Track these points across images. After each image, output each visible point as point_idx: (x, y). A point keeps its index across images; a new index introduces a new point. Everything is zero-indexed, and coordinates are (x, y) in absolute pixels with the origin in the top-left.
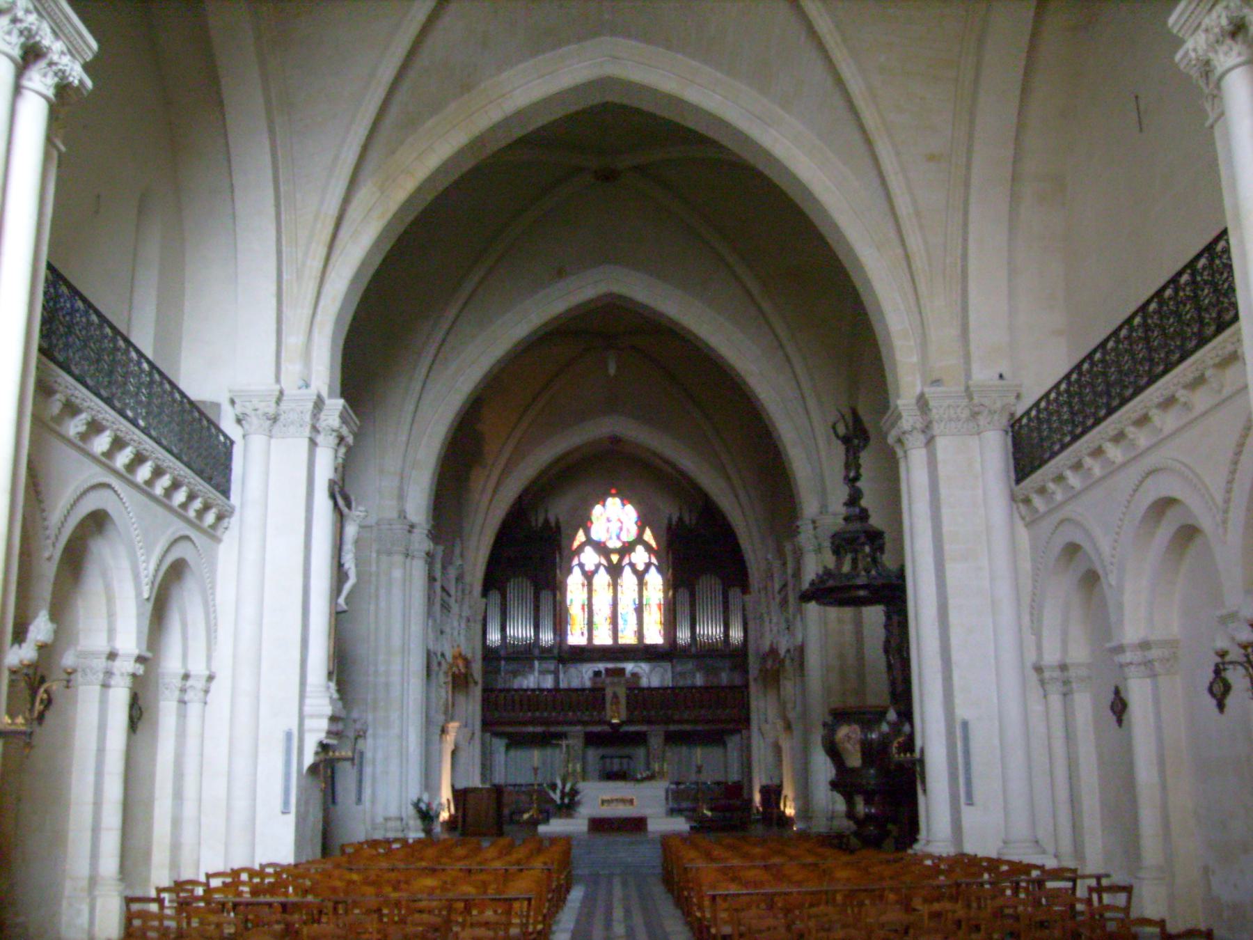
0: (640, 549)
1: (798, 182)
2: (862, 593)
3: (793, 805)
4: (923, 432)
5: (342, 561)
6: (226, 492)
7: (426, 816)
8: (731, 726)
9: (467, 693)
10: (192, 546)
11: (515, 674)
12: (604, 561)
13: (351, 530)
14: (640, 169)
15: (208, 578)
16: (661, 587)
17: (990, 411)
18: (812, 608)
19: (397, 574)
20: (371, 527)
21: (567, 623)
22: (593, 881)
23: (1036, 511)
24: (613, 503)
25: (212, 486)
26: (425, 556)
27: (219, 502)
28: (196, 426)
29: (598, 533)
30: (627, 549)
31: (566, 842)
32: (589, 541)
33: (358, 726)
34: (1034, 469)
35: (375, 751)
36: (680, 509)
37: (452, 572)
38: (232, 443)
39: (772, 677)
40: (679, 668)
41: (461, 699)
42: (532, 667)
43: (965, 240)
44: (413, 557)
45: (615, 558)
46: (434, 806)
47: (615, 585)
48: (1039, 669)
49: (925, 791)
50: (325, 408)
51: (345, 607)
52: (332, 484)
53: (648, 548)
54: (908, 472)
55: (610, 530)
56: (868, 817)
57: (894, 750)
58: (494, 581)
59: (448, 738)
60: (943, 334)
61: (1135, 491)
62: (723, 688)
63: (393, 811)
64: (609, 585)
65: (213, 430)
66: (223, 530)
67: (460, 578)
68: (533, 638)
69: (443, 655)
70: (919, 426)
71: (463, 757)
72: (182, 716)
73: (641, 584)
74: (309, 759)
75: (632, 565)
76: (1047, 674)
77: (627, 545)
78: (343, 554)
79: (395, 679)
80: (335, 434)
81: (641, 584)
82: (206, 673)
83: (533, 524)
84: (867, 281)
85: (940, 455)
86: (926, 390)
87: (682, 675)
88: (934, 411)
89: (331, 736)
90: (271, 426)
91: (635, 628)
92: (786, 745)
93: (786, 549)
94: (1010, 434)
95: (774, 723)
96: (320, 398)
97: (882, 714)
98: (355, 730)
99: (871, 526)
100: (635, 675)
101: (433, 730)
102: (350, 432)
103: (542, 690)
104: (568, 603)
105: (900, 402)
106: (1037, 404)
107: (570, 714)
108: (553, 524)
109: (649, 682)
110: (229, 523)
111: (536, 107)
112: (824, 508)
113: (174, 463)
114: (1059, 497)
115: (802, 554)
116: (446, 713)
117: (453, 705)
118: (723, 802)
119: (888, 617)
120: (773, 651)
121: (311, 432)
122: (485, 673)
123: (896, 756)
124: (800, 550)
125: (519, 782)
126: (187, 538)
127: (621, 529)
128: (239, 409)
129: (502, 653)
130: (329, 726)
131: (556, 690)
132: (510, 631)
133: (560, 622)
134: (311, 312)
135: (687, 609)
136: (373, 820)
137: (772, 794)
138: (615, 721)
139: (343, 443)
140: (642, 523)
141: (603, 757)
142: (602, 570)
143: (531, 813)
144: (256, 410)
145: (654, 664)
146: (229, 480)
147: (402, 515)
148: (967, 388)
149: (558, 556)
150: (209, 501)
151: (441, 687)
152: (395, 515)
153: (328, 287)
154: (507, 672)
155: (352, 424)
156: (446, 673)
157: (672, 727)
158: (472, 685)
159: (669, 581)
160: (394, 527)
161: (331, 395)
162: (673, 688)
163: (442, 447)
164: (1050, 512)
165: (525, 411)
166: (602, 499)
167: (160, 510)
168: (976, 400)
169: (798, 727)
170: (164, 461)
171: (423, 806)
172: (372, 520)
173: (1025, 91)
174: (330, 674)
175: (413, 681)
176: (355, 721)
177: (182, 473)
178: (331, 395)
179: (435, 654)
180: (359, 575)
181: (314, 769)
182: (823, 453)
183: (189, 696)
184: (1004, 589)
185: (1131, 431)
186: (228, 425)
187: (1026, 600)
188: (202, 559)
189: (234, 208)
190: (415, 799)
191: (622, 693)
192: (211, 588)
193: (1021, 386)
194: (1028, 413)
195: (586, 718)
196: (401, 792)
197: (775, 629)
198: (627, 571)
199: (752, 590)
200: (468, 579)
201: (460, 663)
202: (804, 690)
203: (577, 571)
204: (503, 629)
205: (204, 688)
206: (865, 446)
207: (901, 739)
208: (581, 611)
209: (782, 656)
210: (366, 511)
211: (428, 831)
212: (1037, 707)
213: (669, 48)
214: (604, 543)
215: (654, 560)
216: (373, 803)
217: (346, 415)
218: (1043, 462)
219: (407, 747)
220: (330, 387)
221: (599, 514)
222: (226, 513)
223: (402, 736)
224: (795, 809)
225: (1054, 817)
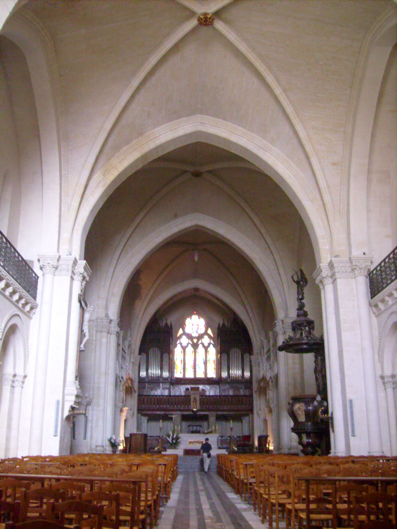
0: (206, 337)
2: (305, 346)
3: (272, 445)
4: (331, 277)
5: (83, 329)
6: (35, 298)
7: (114, 445)
8: (245, 412)
9: (131, 396)
11: (152, 389)
13: (87, 316)
15: (26, 333)
16: (215, 353)
17: (360, 268)
18: (282, 354)
19: (104, 340)
21: (174, 368)
22: (187, 473)
23: (380, 309)
24: (195, 317)
25: (29, 294)
26: (116, 333)
27: (32, 301)
28: (24, 268)
29: (188, 329)
30: (200, 337)
31: (176, 457)
32: (184, 333)
33: (88, 399)
34: (379, 292)
35: (92, 416)
36: (223, 320)
37: (127, 343)
38: (38, 277)
39: (263, 391)
40: (222, 388)
41: (129, 399)
42: (159, 386)
44: (111, 334)
45: (195, 341)
46: (118, 441)
47: (195, 352)
48: (382, 377)
49: (333, 431)
50: (78, 264)
51: (84, 349)
52: (80, 296)
54: (325, 294)
55: (193, 329)
56: (308, 444)
57: (320, 413)
58: (143, 349)
59: (123, 414)
60: (339, 236)
62: (242, 396)
63: (100, 443)
64: (192, 352)
65: (31, 271)
66: (33, 314)
67: (130, 346)
68: (160, 373)
69: (122, 378)
70: (329, 275)
71: (129, 423)
72: (12, 393)
73: (206, 351)
74: (66, 413)
75: (203, 344)
76: (386, 380)
77: (200, 335)
78: (83, 326)
79: (102, 385)
80: (81, 275)
81: (206, 351)
82: (24, 374)
83: (161, 325)
84: (307, 215)
85: (339, 287)
86: (333, 259)
87: (224, 390)
88: (336, 268)
89: (76, 404)
90: (55, 270)
91: (204, 370)
92: (268, 419)
93: (270, 335)
94: (368, 278)
95: (264, 410)
96: (75, 259)
97: (314, 398)
98: (87, 401)
99: (308, 318)
100: (203, 390)
101: (118, 410)
102: (88, 275)
103: (163, 396)
105: (321, 265)
106: (380, 264)
107: (175, 406)
108: (169, 325)
109: (209, 393)
110: (35, 311)
111: (168, 143)
112: (287, 315)
113: (14, 282)
114: (390, 303)
115: (277, 335)
116: (123, 402)
117: (126, 400)
118: (242, 442)
119: (316, 357)
120: (264, 378)
121: (72, 274)
122: (139, 388)
123: (321, 415)
124: (276, 333)
125: (152, 435)
126: (18, 315)
127: (198, 328)
128: (41, 263)
129: (147, 380)
130: (75, 399)
131: (170, 396)
132: (150, 371)
133: (171, 369)
134: (73, 224)
135: (226, 363)
136: (91, 446)
137: (263, 439)
138: (194, 410)
139: (85, 279)
141: (189, 426)
143: (158, 447)
145: (212, 386)
146: (36, 293)
147: (107, 316)
148: (350, 258)
150: (28, 300)
151: (121, 391)
152: (104, 315)
153: (80, 214)
154: (148, 388)
155: (89, 272)
156: (123, 385)
157: (219, 413)
158: (133, 392)
159: (218, 351)
160: (103, 320)
162: (220, 396)
163: (124, 288)
164: (386, 310)
165: (158, 277)
166: (190, 316)
167: (8, 303)
168: (354, 264)
169: (274, 413)
170: (10, 280)
171: (113, 441)
172: (94, 318)
173: (373, 135)
174: (76, 377)
175: (109, 386)
176: (86, 398)
177: (17, 287)
179: (119, 377)
180: (90, 335)
181: (68, 418)
182: (287, 294)
183: (16, 384)
184: (367, 343)
186: (36, 269)
187: (376, 348)
188: (24, 325)
189: (42, 180)
190: (109, 438)
191: (198, 398)
192: (27, 338)
193: (373, 258)
194: (376, 268)
195: (182, 408)
196: (103, 435)
197: (265, 369)
198: (200, 346)
199: (254, 354)
200: (133, 347)
201: (129, 382)
202: (278, 393)
204: (147, 370)
205: (22, 381)
207: (323, 408)
209: (268, 380)
210: (94, 308)
211: (114, 452)
212: (382, 394)
213: (224, 119)
214: (191, 334)
215: (212, 342)
216: (91, 438)
217: (86, 267)
218: (383, 288)
219: (107, 415)
220: (80, 256)
221: (188, 321)
222: (35, 307)
223: (104, 411)
224: (273, 446)
225: (390, 442)
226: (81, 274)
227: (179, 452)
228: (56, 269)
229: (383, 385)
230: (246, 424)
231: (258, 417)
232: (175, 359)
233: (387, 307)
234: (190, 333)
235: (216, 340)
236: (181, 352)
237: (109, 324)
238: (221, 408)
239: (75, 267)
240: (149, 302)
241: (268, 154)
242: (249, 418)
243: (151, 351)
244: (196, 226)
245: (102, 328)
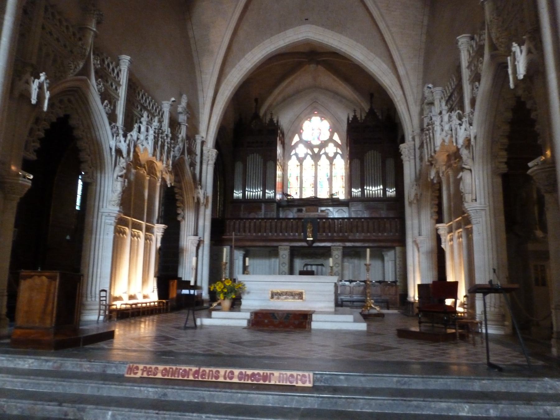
24: (316, 120)
30: (323, 145)
32: (301, 141)
45: (316, 150)
47: (316, 165)
53: (336, 145)
75: (326, 154)
107: (281, 234)
142: (309, 157)
149: (279, 150)
157: (348, 244)
166: (309, 117)
197: (447, 127)
198: (323, 157)
214: (310, 142)
215: (339, 151)
230: (390, 262)
231: (416, 250)
232: (289, 175)
234: (309, 140)
235: (345, 148)
236: (297, 166)
238: (350, 238)
242: (395, 254)
243: (250, 158)
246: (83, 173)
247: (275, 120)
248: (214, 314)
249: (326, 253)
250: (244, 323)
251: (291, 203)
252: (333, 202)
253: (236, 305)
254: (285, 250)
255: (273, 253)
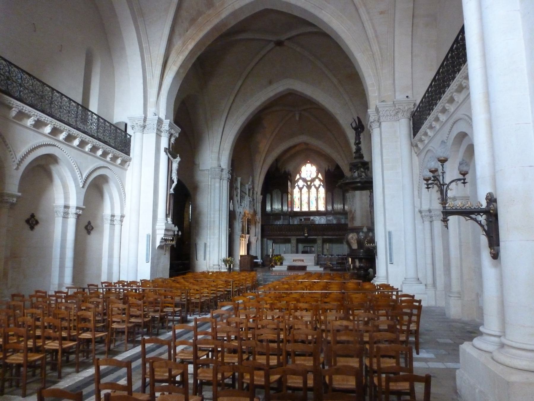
0: (317, 180)
1: (332, 30)
2: (359, 185)
10: (109, 170)
12: (305, 184)
14: (289, 39)
19: (217, 185)
20: (208, 170)
24: (309, 166)
29: (303, 175)
30: (313, 180)
43: (394, 43)
47: (309, 192)
48: (420, 212)
53: (320, 180)
56: (360, 268)
61: (450, 132)
70: (377, 119)
74: (158, 244)
75: (315, 185)
80: (168, 132)
88: (381, 112)
104: (294, 198)
110: (129, 164)
123: (367, 244)
140: (318, 171)
141: (304, 247)
142: (305, 187)
144: (137, 124)
149: (289, 183)
152: (217, 166)
161: (166, 118)
166: (305, 163)
178: (166, 118)
185: (447, 106)
198: (313, 187)
203: (297, 187)
206: (362, 132)
208: (298, 200)
215: (322, 184)
226: (167, 131)
227: (284, 268)
228: (144, 128)
229: (421, 219)
233: (425, 145)
237: (221, 172)
239: (161, 126)
240: (266, 154)
241: (324, 12)
244: (288, 89)
245: (215, 175)
246: (377, 293)
247: (287, 171)
248: (212, 298)
249: (314, 241)
250: (286, 269)
251: (297, 214)
252: (318, 213)
253: (281, 264)
254: (294, 240)
255: (288, 241)
